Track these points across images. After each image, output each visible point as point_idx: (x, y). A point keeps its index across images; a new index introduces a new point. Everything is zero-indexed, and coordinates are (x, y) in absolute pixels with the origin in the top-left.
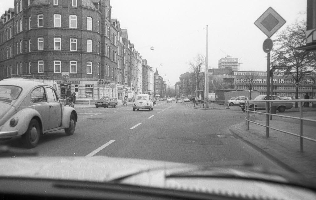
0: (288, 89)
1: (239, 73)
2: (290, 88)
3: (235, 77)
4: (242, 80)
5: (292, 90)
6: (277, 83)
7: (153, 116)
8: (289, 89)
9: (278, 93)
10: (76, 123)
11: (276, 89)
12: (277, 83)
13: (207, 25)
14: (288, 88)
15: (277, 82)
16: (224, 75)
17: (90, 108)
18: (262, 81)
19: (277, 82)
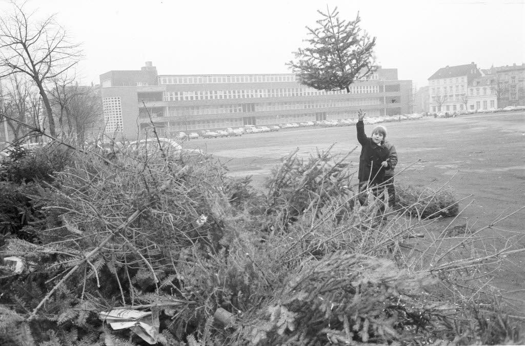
0: (233, 112)
1: (212, 78)
2: (311, 105)
3: (165, 89)
4: (219, 93)
5: (322, 109)
6: (194, 99)
7: (372, 161)
8: (309, 106)
9: (259, 118)
10: (16, 266)
11: (253, 110)
12: (194, 99)
13: (359, 11)
14: (233, 109)
15: (223, 97)
16: (140, 85)
17: (244, 170)
18: (194, 96)
19: (223, 97)
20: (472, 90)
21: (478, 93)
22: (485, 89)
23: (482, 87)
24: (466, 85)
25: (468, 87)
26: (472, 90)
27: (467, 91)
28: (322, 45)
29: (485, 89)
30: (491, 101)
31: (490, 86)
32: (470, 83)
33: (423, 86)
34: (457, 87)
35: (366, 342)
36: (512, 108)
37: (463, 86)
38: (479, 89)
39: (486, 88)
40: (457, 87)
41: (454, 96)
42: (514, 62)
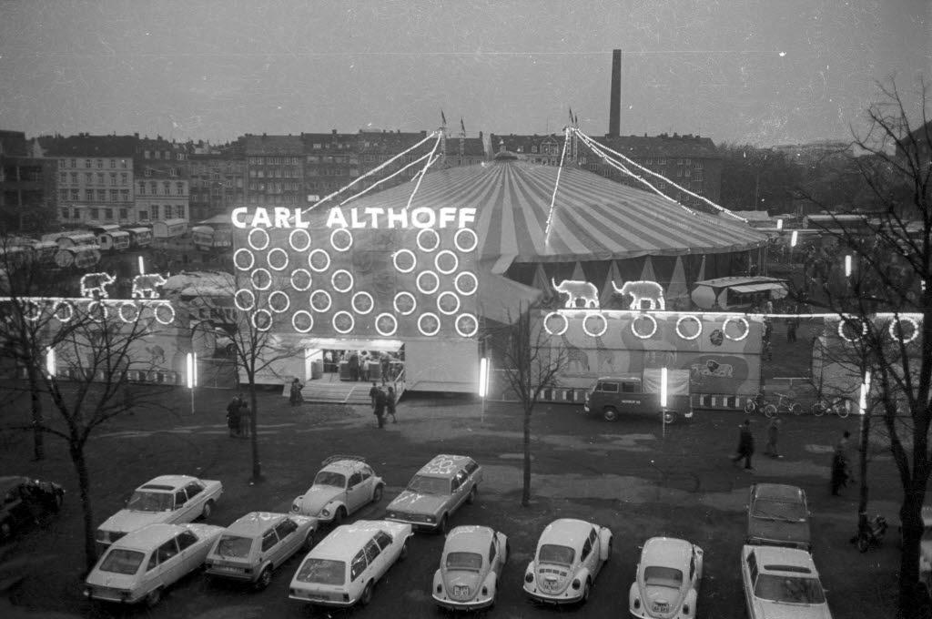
20: (142, 185)
21: (154, 191)
22: (167, 185)
23: (162, 181)
24: (130, 174)
25: (134, 179)
26: (142, 185)
27: (132, 184)
28: (649, 449)
29: (167, 185)
30: (166, 206)
31: (177, 181)
32: (138, 171)
33: (253, 134)
34: (113, 175)
35: (216, 343)
36: (720, 355)
37: (124, 175)
38: (169, 183)
39: (182, 184)
40: (113, 175)
41: (107, 192)
42: (136, 131)
